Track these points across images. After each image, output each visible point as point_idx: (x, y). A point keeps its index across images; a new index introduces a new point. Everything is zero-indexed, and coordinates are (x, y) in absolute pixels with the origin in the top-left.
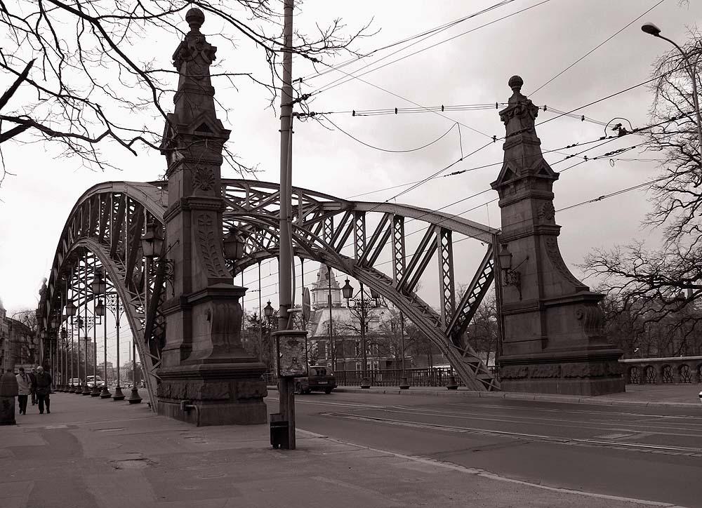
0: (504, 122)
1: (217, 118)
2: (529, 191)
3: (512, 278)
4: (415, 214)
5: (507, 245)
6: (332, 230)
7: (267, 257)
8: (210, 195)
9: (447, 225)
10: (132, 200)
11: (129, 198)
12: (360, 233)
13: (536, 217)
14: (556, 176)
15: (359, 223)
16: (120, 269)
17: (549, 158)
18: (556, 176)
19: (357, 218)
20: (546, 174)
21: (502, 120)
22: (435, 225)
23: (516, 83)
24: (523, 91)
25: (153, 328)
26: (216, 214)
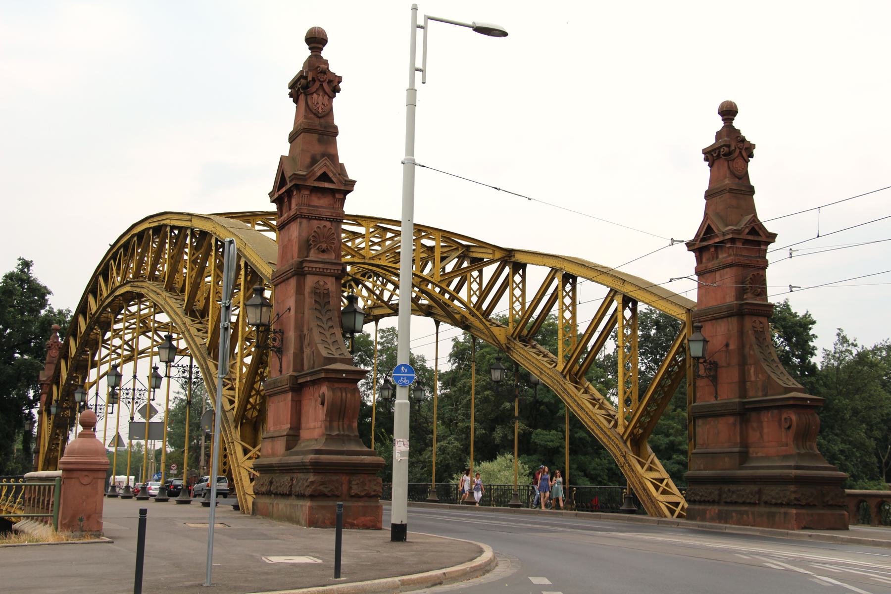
0: (708, 163)
1: (340, 161)
2: (732, 257)
3: (705, 369)
4: (592, 274)
5: (701, 327)
6: (480, 284)
7: (389, 315)
8: (332, 257)
9: (634, 294)
10: (220, 242)
11: (217, 240)
12: (518, 292)
13: (741, 293)
14: (772, 237)
15: (517, 278)
16: (199, 330)
17: (763, 215)
18: (772, 237)
19: (515, 271)
20: (758, 234)
21: (706, 160)
22: (616, 292)
23: (728, 112)
24: (737, 123)
25: (245, 410)
26: (334, 279)
